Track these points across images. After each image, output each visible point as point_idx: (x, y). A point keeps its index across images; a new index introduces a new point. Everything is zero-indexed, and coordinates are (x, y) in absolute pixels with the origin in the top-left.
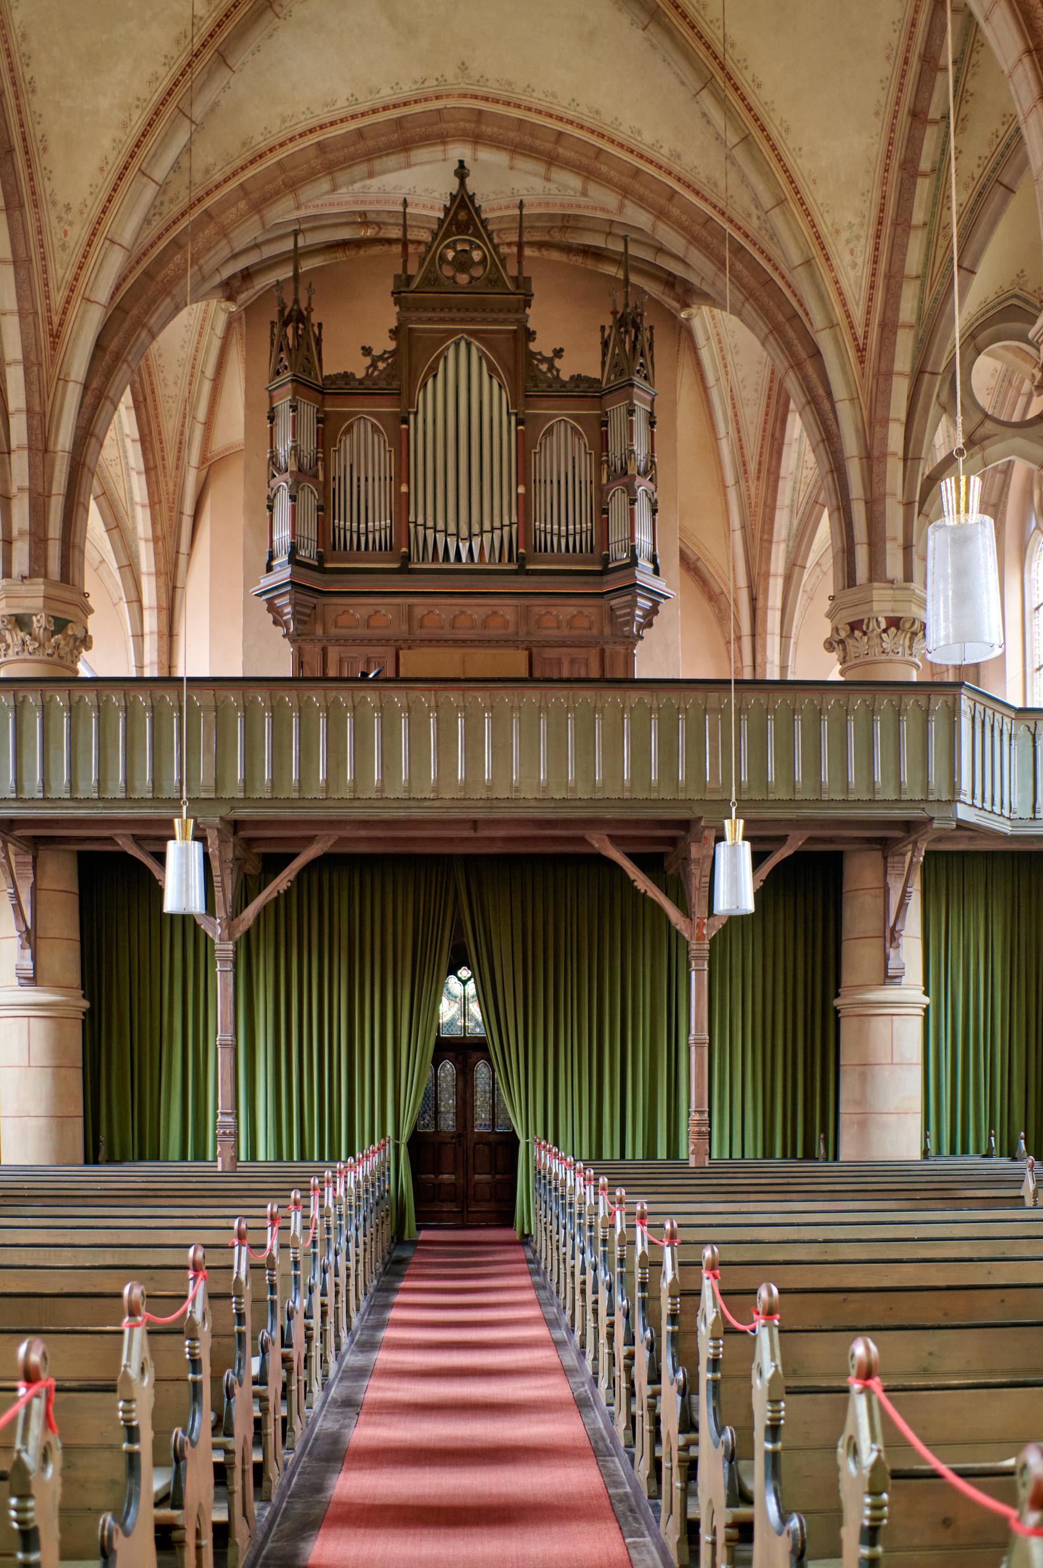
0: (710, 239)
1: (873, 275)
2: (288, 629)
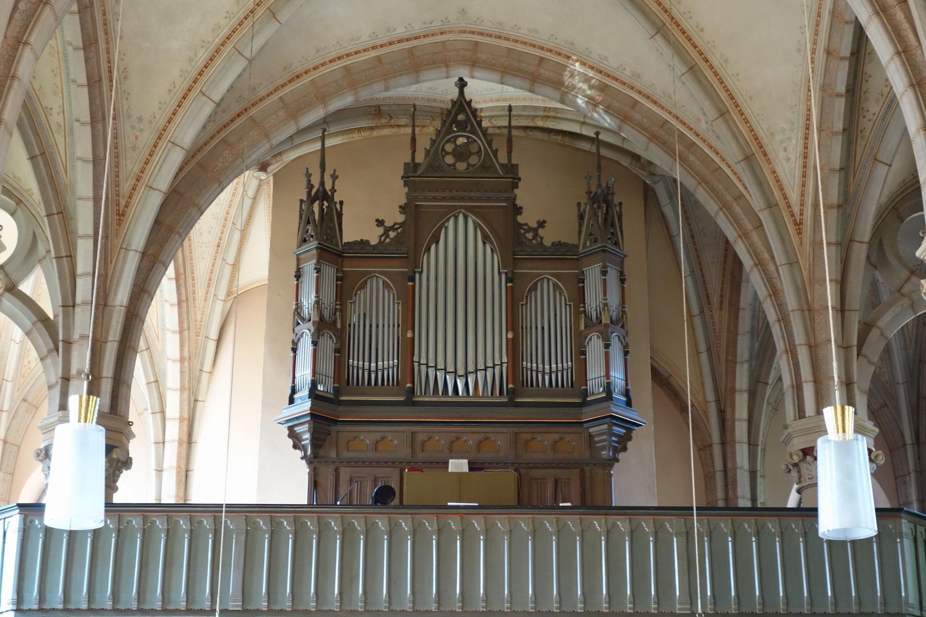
0: (667, 137)
1: (805, 167)
2: (305, 452)
